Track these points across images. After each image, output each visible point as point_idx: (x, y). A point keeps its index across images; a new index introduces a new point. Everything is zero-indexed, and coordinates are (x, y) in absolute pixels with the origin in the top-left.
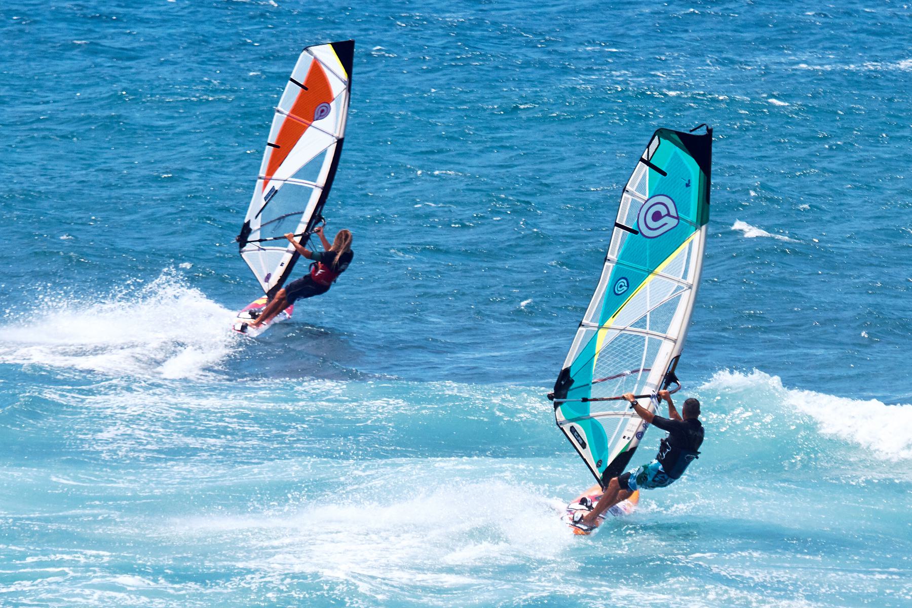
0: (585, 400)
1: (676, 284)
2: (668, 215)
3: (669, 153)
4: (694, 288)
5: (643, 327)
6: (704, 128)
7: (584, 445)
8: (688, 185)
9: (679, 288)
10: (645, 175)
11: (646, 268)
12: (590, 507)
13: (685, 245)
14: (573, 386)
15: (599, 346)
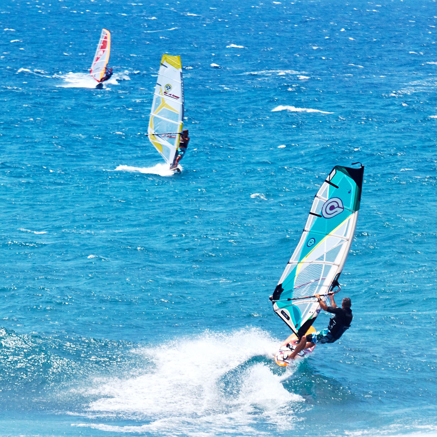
0: (289, 300)
1: (341, 239)
2: (338, 207)
3: (341, 177)
4: (350, 241)
5: (322, 260)
6: (359, 164)
7: (288, 318)
8: (349, 192)
9: (342, 241)
10: (326, 190)
11: (325, 233)
12: (292, 349)
13: (346, 221)
14: (284, 291)
15: (298, 272)
